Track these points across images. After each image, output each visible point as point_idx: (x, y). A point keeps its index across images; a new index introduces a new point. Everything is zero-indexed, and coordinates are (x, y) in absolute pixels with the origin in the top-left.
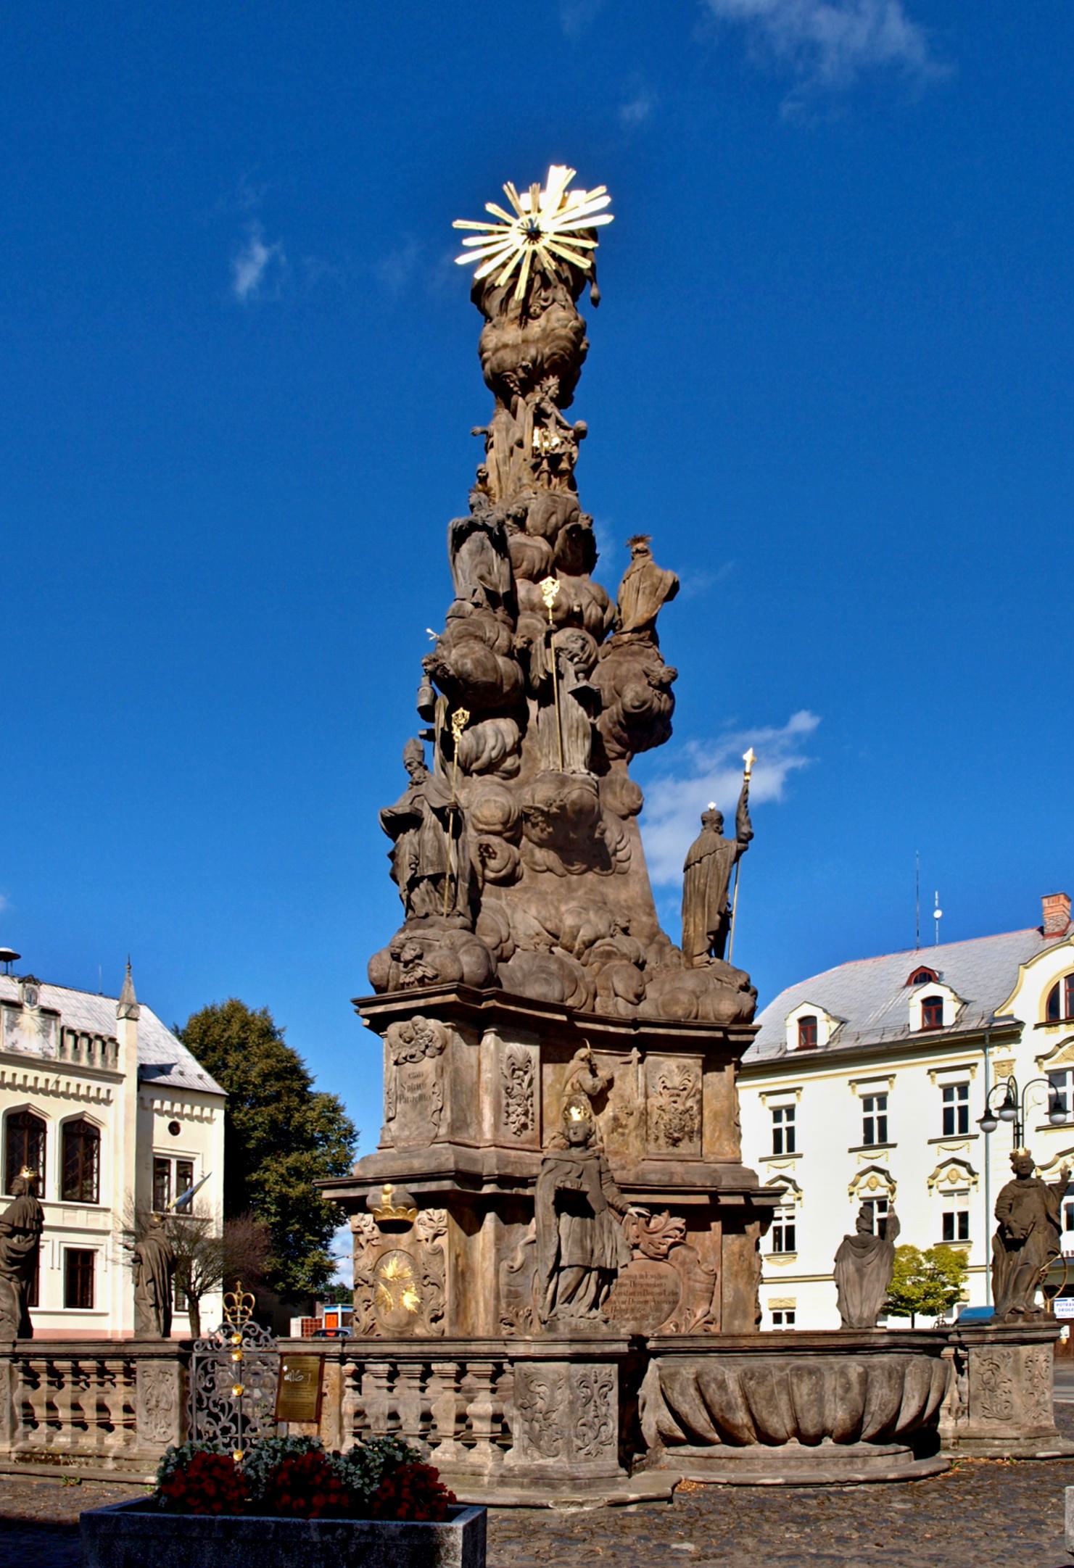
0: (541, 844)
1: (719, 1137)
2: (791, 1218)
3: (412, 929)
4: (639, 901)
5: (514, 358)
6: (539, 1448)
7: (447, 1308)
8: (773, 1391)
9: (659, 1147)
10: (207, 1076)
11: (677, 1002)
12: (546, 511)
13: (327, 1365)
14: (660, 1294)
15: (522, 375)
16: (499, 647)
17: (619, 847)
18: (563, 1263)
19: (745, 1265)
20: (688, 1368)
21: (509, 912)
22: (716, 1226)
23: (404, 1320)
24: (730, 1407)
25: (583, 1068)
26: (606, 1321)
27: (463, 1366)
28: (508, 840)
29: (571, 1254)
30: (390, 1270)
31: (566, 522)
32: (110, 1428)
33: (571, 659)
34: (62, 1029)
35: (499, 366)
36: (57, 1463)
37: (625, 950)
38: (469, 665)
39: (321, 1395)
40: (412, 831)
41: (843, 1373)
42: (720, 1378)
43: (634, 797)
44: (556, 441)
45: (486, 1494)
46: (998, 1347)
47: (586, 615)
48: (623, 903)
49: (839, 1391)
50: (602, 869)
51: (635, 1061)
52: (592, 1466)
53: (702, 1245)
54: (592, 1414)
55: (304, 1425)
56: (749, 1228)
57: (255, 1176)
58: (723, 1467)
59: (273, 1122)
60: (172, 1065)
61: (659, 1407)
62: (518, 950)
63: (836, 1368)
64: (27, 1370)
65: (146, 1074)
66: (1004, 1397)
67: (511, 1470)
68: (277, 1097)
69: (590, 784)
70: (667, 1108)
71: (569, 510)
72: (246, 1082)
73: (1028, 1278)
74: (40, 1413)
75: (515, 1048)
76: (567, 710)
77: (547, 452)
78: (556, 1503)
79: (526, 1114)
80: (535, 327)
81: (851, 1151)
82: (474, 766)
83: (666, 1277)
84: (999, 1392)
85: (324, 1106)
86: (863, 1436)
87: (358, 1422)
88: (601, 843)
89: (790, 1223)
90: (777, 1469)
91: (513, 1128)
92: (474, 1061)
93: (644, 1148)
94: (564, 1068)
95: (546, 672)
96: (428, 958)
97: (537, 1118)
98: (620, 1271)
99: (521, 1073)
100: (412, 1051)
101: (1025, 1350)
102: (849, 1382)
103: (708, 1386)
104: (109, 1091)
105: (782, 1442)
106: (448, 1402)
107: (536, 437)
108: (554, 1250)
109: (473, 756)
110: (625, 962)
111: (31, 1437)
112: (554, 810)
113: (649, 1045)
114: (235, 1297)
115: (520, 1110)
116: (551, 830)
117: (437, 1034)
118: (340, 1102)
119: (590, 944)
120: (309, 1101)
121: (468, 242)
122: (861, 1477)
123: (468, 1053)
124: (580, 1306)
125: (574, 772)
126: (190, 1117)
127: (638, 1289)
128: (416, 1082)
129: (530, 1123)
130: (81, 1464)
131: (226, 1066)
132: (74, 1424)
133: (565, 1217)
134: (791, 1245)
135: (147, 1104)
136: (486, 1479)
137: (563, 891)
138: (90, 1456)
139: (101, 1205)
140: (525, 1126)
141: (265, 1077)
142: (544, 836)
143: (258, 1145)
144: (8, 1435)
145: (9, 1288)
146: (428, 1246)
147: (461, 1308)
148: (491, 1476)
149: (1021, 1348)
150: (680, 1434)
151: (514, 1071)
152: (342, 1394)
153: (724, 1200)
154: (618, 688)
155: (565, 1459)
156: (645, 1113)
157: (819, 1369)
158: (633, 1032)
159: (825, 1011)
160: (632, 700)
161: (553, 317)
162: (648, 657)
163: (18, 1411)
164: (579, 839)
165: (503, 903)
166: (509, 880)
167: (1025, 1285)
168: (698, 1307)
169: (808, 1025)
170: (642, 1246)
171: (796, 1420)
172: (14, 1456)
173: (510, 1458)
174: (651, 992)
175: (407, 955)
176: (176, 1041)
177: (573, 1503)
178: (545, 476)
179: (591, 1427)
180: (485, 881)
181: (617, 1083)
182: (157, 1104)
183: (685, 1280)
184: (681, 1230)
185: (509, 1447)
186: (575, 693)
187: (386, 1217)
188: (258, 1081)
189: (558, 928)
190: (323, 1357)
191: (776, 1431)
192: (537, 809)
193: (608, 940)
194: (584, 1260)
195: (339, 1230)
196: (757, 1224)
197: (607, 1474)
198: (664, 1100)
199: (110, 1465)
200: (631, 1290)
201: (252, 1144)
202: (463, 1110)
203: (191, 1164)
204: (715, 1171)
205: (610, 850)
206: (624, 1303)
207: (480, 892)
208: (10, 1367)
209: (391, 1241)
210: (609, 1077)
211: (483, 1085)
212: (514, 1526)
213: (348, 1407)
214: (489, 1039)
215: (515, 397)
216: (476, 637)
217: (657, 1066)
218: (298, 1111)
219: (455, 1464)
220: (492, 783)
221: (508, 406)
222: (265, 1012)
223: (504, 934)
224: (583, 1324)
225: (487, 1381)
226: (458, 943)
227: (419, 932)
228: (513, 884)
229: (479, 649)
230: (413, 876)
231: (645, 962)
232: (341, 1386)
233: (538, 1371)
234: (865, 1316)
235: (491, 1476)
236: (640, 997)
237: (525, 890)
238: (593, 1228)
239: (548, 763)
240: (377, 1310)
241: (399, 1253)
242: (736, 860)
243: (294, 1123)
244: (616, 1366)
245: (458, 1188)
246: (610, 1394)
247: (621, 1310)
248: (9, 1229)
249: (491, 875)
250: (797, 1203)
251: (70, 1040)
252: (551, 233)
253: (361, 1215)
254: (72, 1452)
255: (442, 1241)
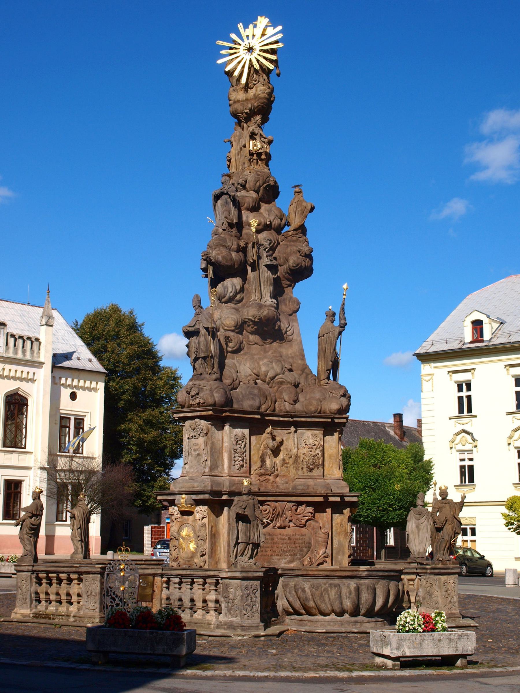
0: (252, 333)
1: (332, 467)
2: (471, 460)
3: (195, 380)
4: (297, 353)
5: (242, 108)
6: (230, 614)
7: (207, 550)
8: (322, 594)
9: (304, 473)
10: (94, 360)
11: (311, 404)
12: (255, 180)
13: (156, 578)
14: (302, 543)
15: (245, 116)
16: (233, 249)
17: (288, 330)
18: (239, 541)
19: (343, 529)
20: (292, 582)
21: (237, 365)
22: (329, 510)
23: (190, 555)
24: (307, 599)
25: (269, 438)
26: (255, 564)
27: (205, 580)
28: (237, 333)
29: (242, 538)
30: (184, 533)
31: (264, 183)
32: (71, 603)
33: (265, 250)
34: (7, 334)
35: (235, 111)
36: (50, 618)
37: (289, 380)
38: (220, 259)
39: (154, 591)
40: (195, 337)
41: (348, 587)
42: (302, 587)
43: (295, 305)
44: (259, 146)
45: (211, 632)
46: (432, 576)
47: (273, 224)
48: (290, 355)
49: (348, 594)
50: (280, 341)
51: (293, 432)
52: (250, 621)
53: (322, 520)
54: (250, 601)
55: (147, 603)
56: (345, 511)
57: (123, 427)
58: (306, 625)
59: (135, 387)
60: (72, 354)
61: (283, 598)
62: (241, 383)
63: (346, 584)
64: (37, 578)
65: (58, 359)
66: (435, 599)
67: (221, 622)
68: (137, 371)
69: (272, 307)
70: (307, 454)
71: (265, 179)
72: (118, 362)
73: (444, 545)
74: (42, 596)
75: (238, 431)
76: (262, 273)
77: (256, 151)
78: (234, 635)
79: (243, 460)
80: (251, 93)
81: (508, 414)
82: (223, 300)
83: (305, 535)
84: (433, 596)
85: (168, 377)
86: (361, 614)
87: (168, 602)
88: (280, 330)
89: (471, 463)
90: (326, 626)
91: (237, 467)
92: (221, 438)
93: (297, 473)
94: (261, 437)
95: (253, 259)
96: (201, 395)
97: (248, 461)
98: (261, 544)
99: (241, 442)
100: (195, 434)
101: (444, 578)
102: (350, 591)
103: (298, 590)
104: (34, 373)
105: (329, 615)
106: (200, 594)
107: (251, 145)
108: (235, 536)
109: (223, 295)
110: (289, 385)
111: (39, 607)
112: (257, 320)
113: (298, 425)
114: (122, 548)
115: (240, 459)
116: (256, 327)
117: (205, 427)
118: (179, 373)
119: (273, 378)
120: (158, 373)
121: (223, 52)
122: (356, 630)
123: (218, 434)
124: (246, 558)
125: (266, 301)
126: (84, 388)
127: (292, 541)
128: (196, 447)
129: (244, 464)
130: (59, 619)
131: (106, 351)
132: (57, 602)
133: (240, 523)
134: (471, 480)
135: (57, 380)
136: (212, 626)
137: (262, 353)
138: (63, 616)
139: (28, 449)
140: (242, 466)
141: (131, 358)
142: (253, 330)
143: (125, 404)
144: (29, 606)
145: (30, 541)
146: (200, 522)
147: (213, 550)
148: (214, 625)
149: (441, 577)
150: (291, 610)
151: (237, 441)
152: (162, 590)
153: (331, 499)
154: (287, 257)
155: (239, 618)
156: (297, 457)
157: (339, 585)
158: (291, 420)
159: (488, 317)
160: (292, 264)
161: (258, 89)
162: (300, 242)
163: (33, 595)
164: (270, 330)
165: (235, 361)
166: (238, 351)
167: (443, 548)
168: (320, 550)
169: (477, 325)
170: (293, 521)
171: (332, 605)
172: (31, 615)
173: (222, 618)
174: (301, 398)
175: (193, 393)
176: (75, 335)
177: (240, 635)
178: (255, 161)
179: (249, 606)
180: (227, 352)
181: (285, 442)
182: (63, 381)
183: (314, 537)
184: (312, 513)
185: (221, 613)
186: (266, 266)
187: (183, 509)
188: (126, 361)
189: (259, 372)
190: (154, 576)
191: (324, 610)
192: (249, 319)
193: (281, 376)
194: (246, 540)
195: (177, 461)
196: (349, 509)
197: (255, 625)
198: (305, 451)
199: (72, 619)
200: (288, 542)
201: (121, 404)
202: (216, 460)
203: (83, 420)
204: (328, 484)
205: (284, 332)
206: (285, 548)
207: (225, 358)
208: (31, 576)
209: (185, 519)
210: (281, 440)
211: (224, 448)
212: (218, 643)
213: (164, 596)
214: (227, 428)
215: (242, 123)
216: (223, 246)
217: (303, 434)
218: (151, 380)
219: (202, 620)
220: (231, 308)
221: (240, 126)
222: (131, 312)
223: (235, 377)
224: (246, 565)
225: (214, 586)
226: (213, 388)
227: (197, 382)
228: (240, 352)
229: (224, 251)
230: (195, 357)
231: (299, 383)
232: (161, 587)
233: (230, 583)
234: (421, 551)
235: (214, 625)
236: (296, 401)
237: (245, 354)
238: (250, 527)
239: (255, 296)
240: (179, 551)
241: (188, 525)
242: (340, 333)
243: (148, 389)
244: (259, 582)
245: (212, 498)
246: (257, 593)
247: (284, 551)
248: (31, 515)
249: (230, 349)
250: (475, 449)
251: (11, 341)
252: (258, 50)
253: (173, 507)
254: (56, 614)
255: (206, 520)
